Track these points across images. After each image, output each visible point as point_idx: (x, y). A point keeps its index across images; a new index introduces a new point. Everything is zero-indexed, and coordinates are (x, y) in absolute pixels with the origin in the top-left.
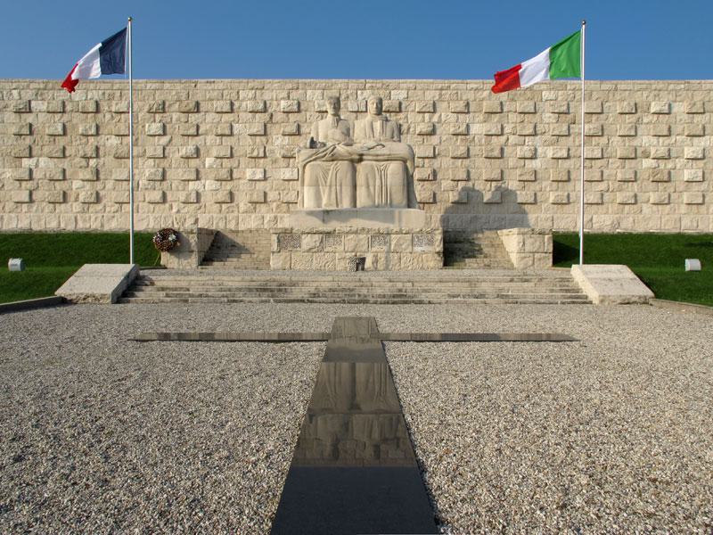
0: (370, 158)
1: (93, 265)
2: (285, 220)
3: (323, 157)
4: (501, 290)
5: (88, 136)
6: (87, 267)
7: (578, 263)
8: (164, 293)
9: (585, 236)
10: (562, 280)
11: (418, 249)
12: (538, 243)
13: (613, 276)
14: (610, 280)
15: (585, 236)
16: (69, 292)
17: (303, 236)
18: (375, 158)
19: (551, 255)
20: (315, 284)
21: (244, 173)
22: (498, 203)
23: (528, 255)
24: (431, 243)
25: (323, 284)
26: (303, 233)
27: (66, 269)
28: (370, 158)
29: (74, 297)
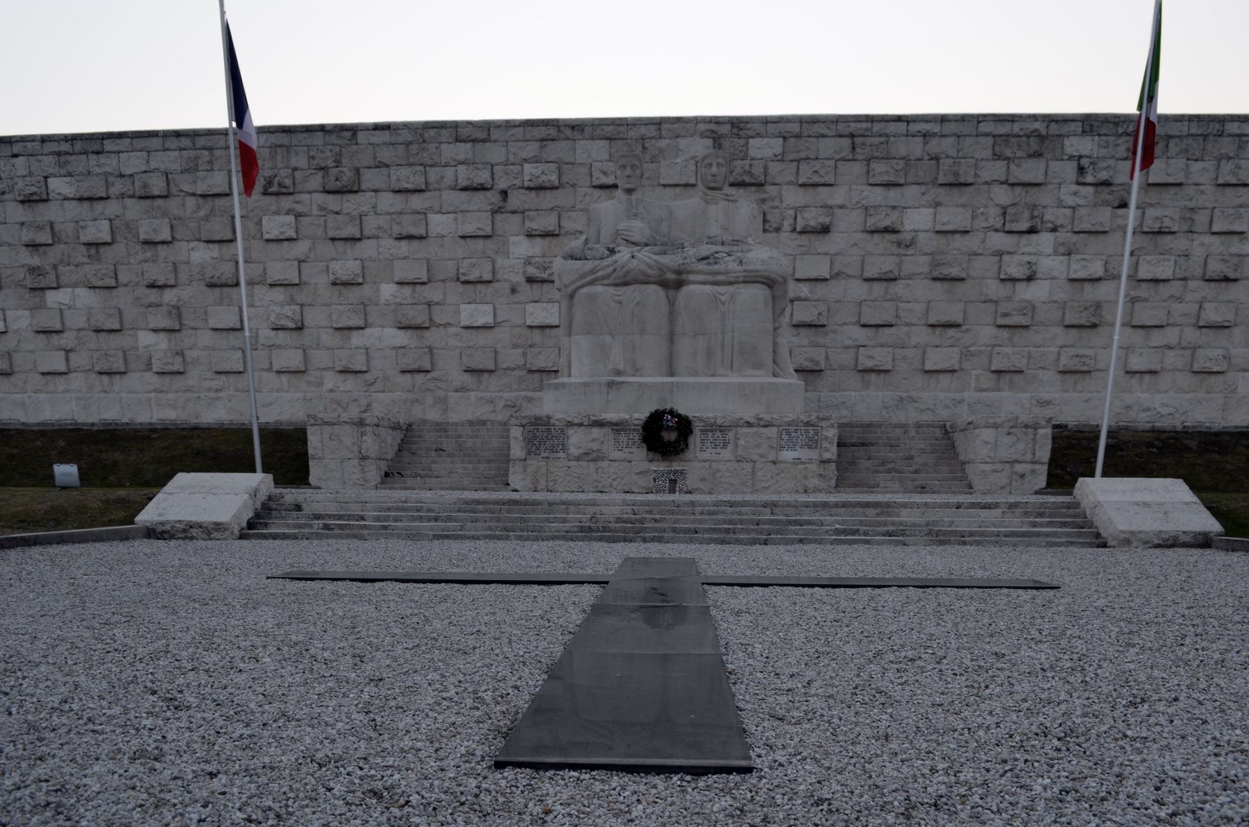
0: (701, 278)
1: (193, 474)
2: (321, 408)
3: (608, 276)
4: (934, 523)
5: (42, 289)
6: (182, 478)
7: (1092, 475)
8: (321, 522)
9: (263, 431)
10: (1069, 506)
11: (788, 455)
12: (1021, 446)
13: (1147, 497)
14: (1146, 504)
15: (263, 431)
16: (157, 519)
17: (571, 431)
18: (710, 278)
19: (1045, 468)
20: (592, 510)
21: (458, 312)
22: (953, 371)
23: (999, 467)
24: (812, 444)
25: (604, 509)
26: (570, 424)
27: (154, 490)
28: (701, 278)
29: (168, 527)
